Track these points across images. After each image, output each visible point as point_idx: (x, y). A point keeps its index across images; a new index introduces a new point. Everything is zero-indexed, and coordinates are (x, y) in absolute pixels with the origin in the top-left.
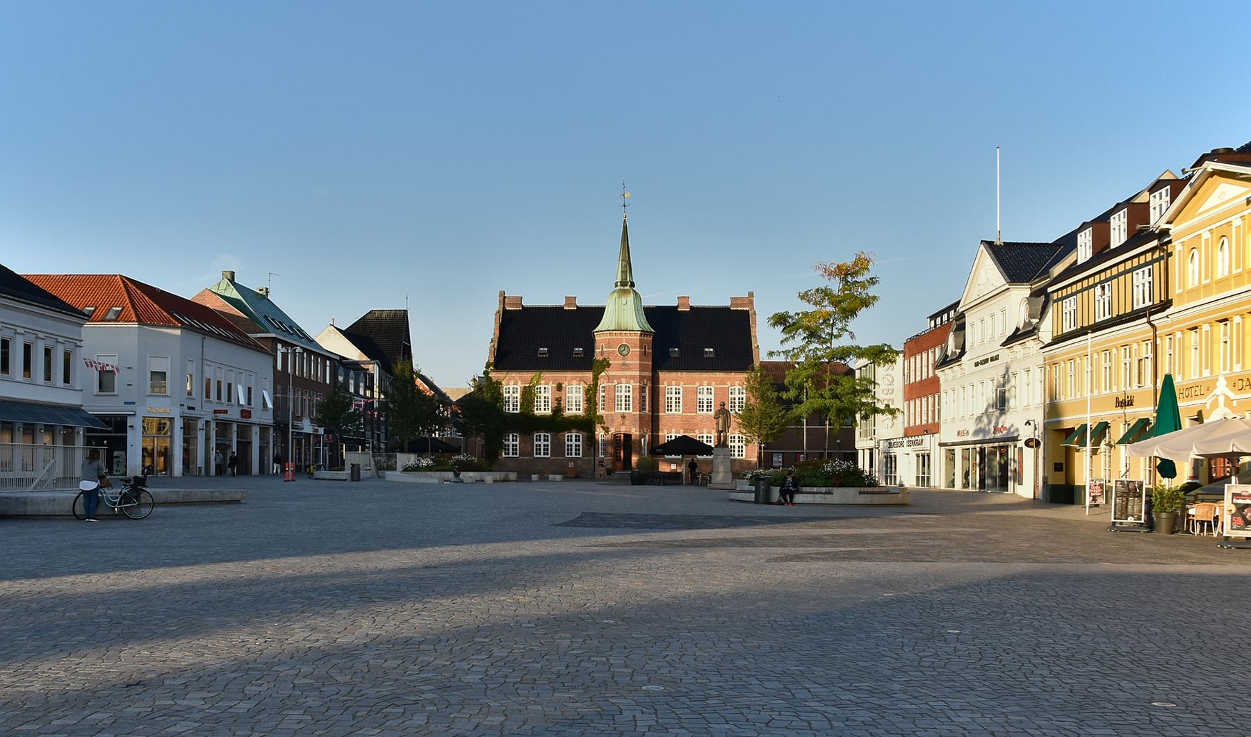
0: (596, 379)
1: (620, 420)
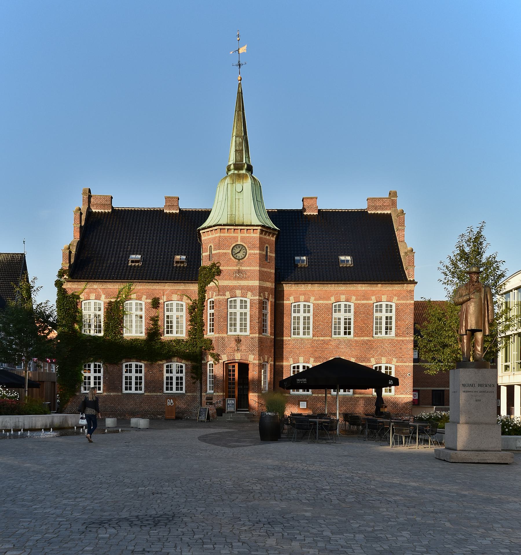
0: (202, 291)
1: (233, 344)
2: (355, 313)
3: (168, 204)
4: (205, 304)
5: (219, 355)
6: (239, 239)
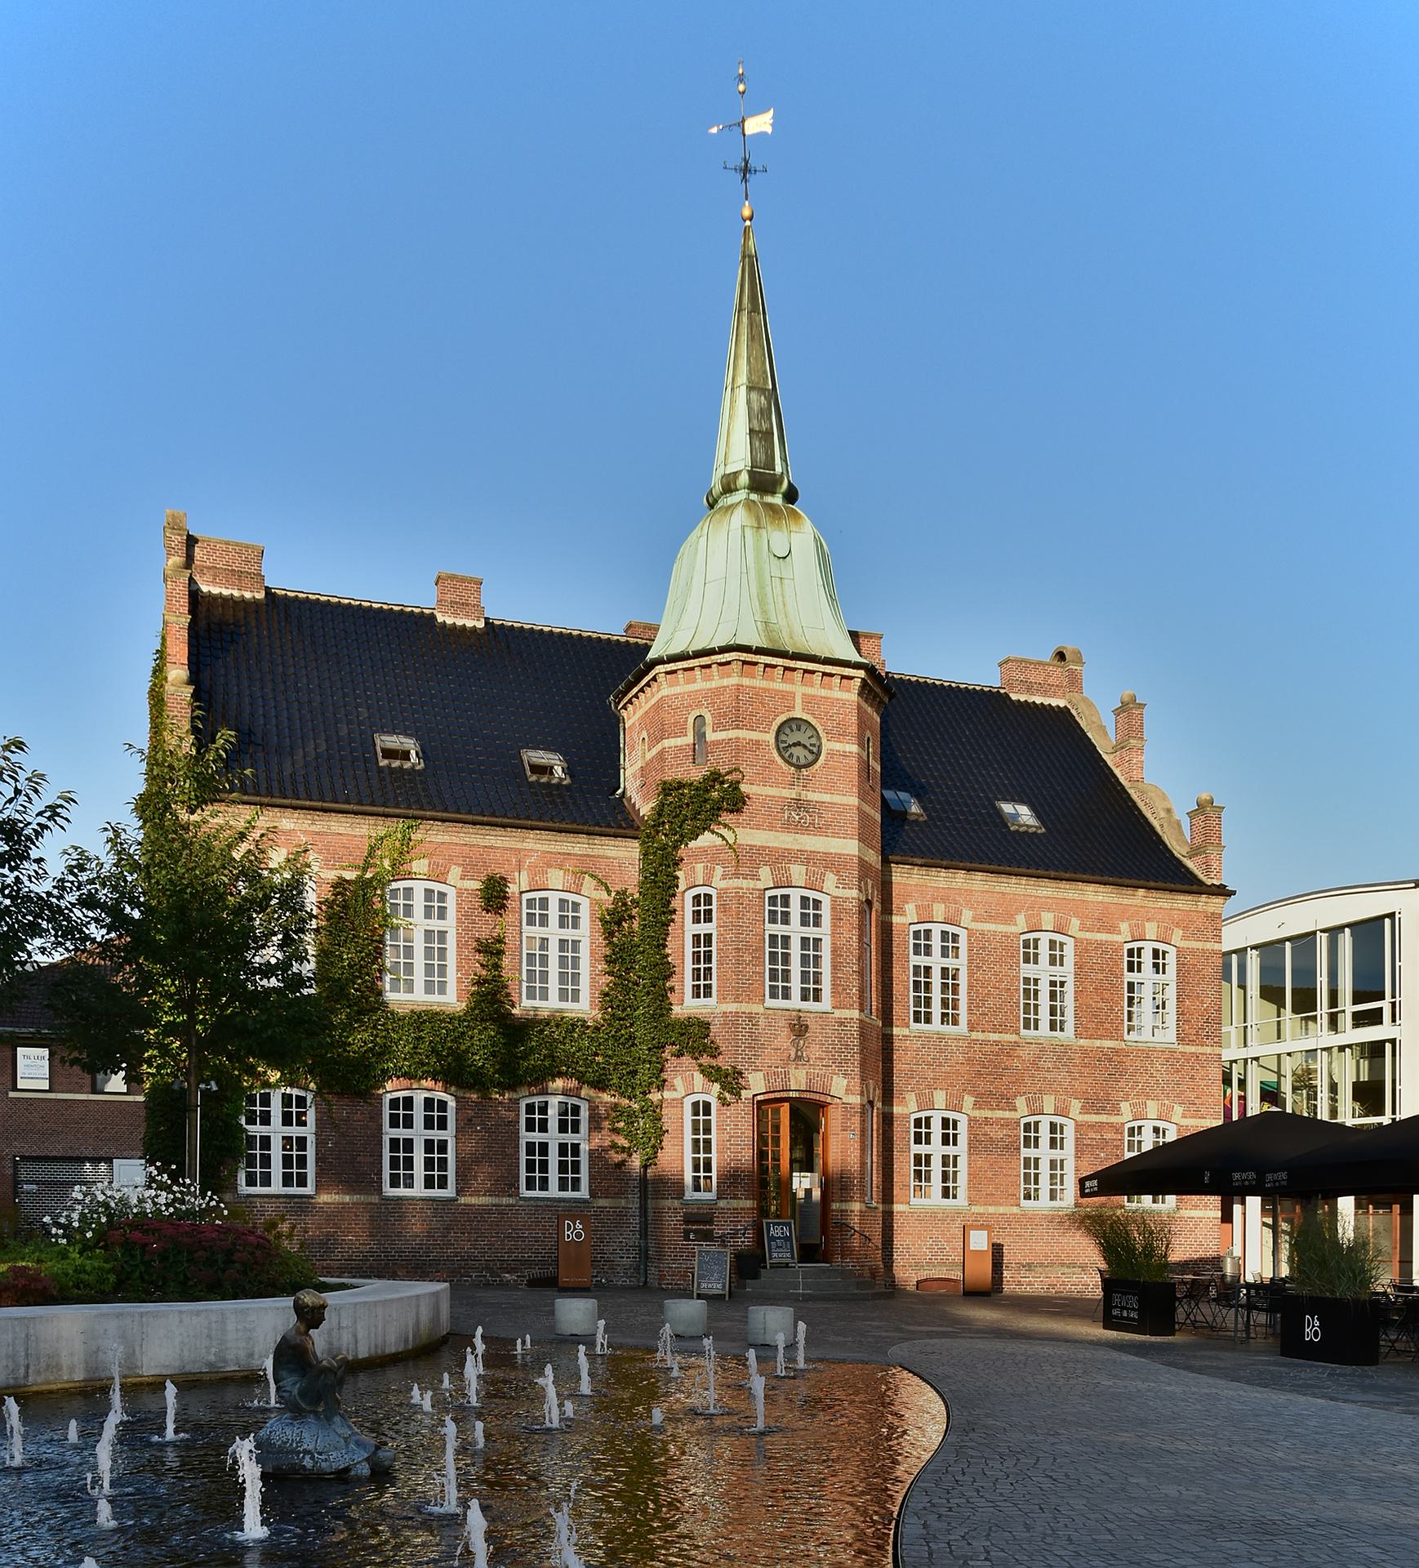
1: (784, 1039)
2: (1079, 966)
3: (448, 597)
4: (675, 903)
5: (740, 1073)
6: (798, 701)
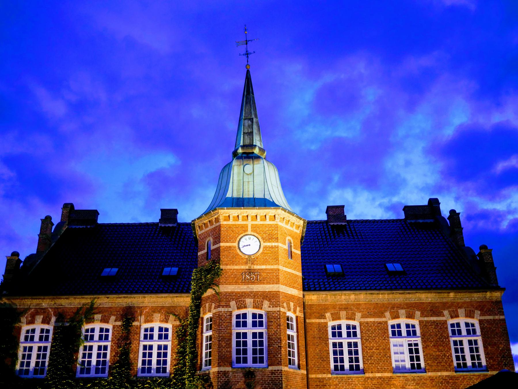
0: (198, 304)
